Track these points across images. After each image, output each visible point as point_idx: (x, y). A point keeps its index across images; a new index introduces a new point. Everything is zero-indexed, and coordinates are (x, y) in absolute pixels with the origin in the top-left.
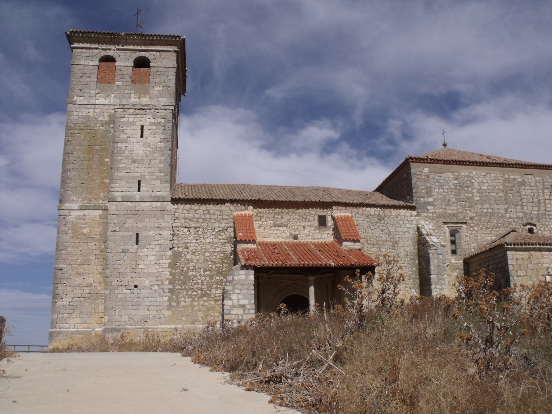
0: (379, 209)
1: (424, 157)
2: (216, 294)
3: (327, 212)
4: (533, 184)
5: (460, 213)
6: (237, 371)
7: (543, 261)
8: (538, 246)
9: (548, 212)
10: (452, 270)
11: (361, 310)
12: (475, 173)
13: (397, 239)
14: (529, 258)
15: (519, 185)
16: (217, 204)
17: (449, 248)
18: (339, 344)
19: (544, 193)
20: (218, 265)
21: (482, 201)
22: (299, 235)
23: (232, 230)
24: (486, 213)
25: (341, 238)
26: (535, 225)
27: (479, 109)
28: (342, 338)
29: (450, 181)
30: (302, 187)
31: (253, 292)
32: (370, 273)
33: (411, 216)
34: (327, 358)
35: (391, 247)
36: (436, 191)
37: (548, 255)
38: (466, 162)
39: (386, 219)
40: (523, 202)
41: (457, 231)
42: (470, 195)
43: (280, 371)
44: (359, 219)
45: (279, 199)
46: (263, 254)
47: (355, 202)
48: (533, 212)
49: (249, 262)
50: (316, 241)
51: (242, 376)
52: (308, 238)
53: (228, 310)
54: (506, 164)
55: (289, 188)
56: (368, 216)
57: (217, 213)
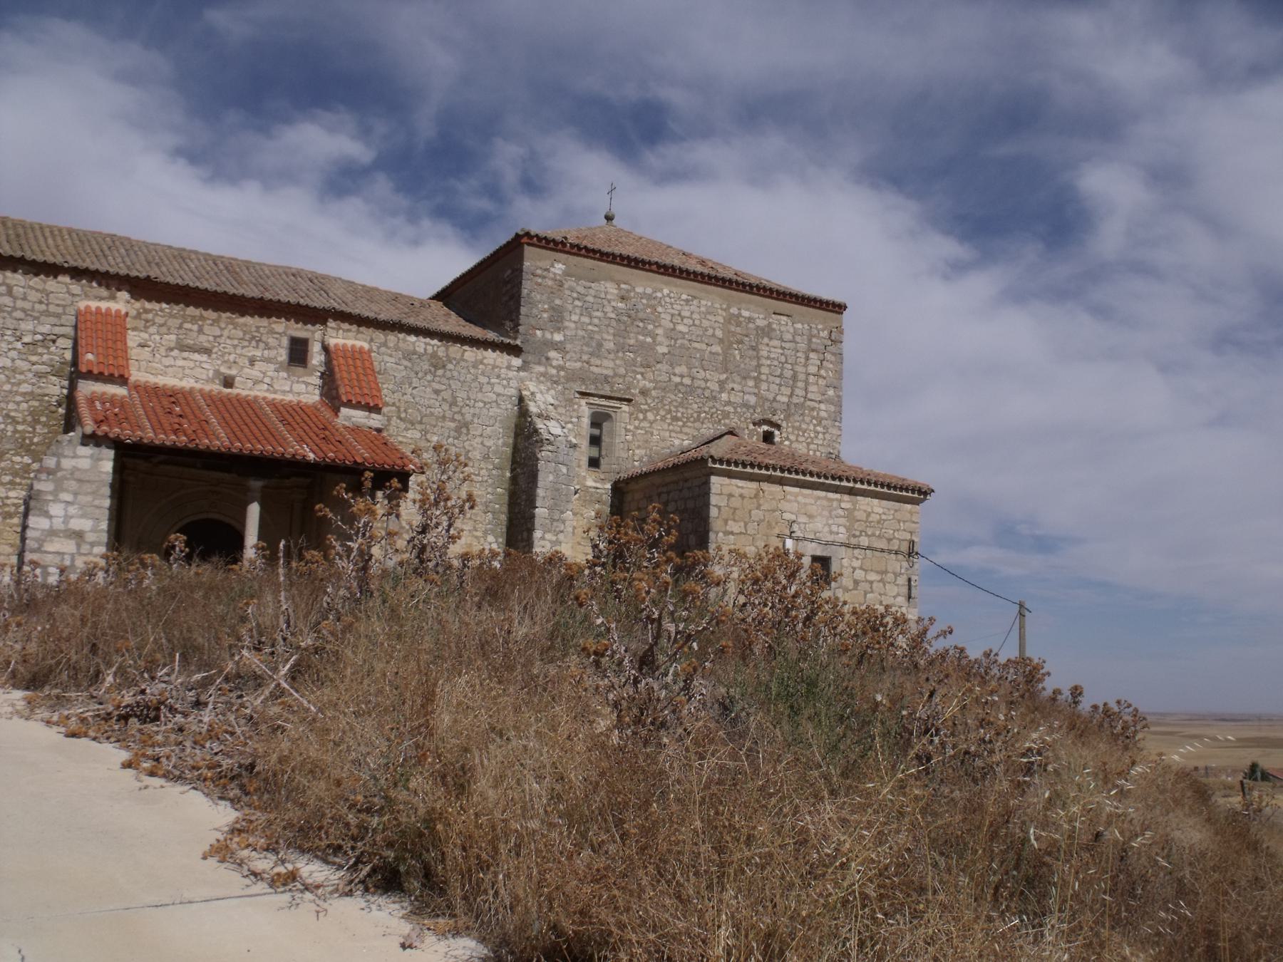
0: (435, 342)
1: (559, 238)
2: (7, 498)
3: (313, 332)
4: (788, 337)
5: (620, 376)
6: (47, 687)
7: (784, 505)
8: (778, 473)
9: (809, 403)
10: (585, 503)
11: (365, 568)
12: (666, 291)
13: (468, 417)
14: (756, 496)
15: (757, 334)
16: (37, 275)
17: (585, 451)
18: (307, 641)
19: (807, 358)
20: (20, 428)
21: (671, 359)
22: (238, 379)
23: (69, 344)
24: (677, 385)
25: (338, 397)
26: (778, 427)
27: (703, 153)
28: (316, 627)
29: (609, 301)
30: (259, 264)
31: (107, 503)
32: (395, 483)
33: (509, 367)
34: (275, 670)
35: (453, 433)
36: (573, 319)
37: (796, 495)
38: (650, 263)
39: (450, 366)
40: (760, 373)
41: (607, 417)
42: (649, 340)
43: (156, 692)
44: (387, 358)
45: (198, 284)
46: (142, 412)
47: (382, 317)
48: (779, 398)
49: (105, 428)
50: (279, 397)
51: (60, 701)
52: (257, 387)
53: (37, 540)
54: (737, 282)
55: (227, 262)
56: (409, 355)
57: (34, 296)
